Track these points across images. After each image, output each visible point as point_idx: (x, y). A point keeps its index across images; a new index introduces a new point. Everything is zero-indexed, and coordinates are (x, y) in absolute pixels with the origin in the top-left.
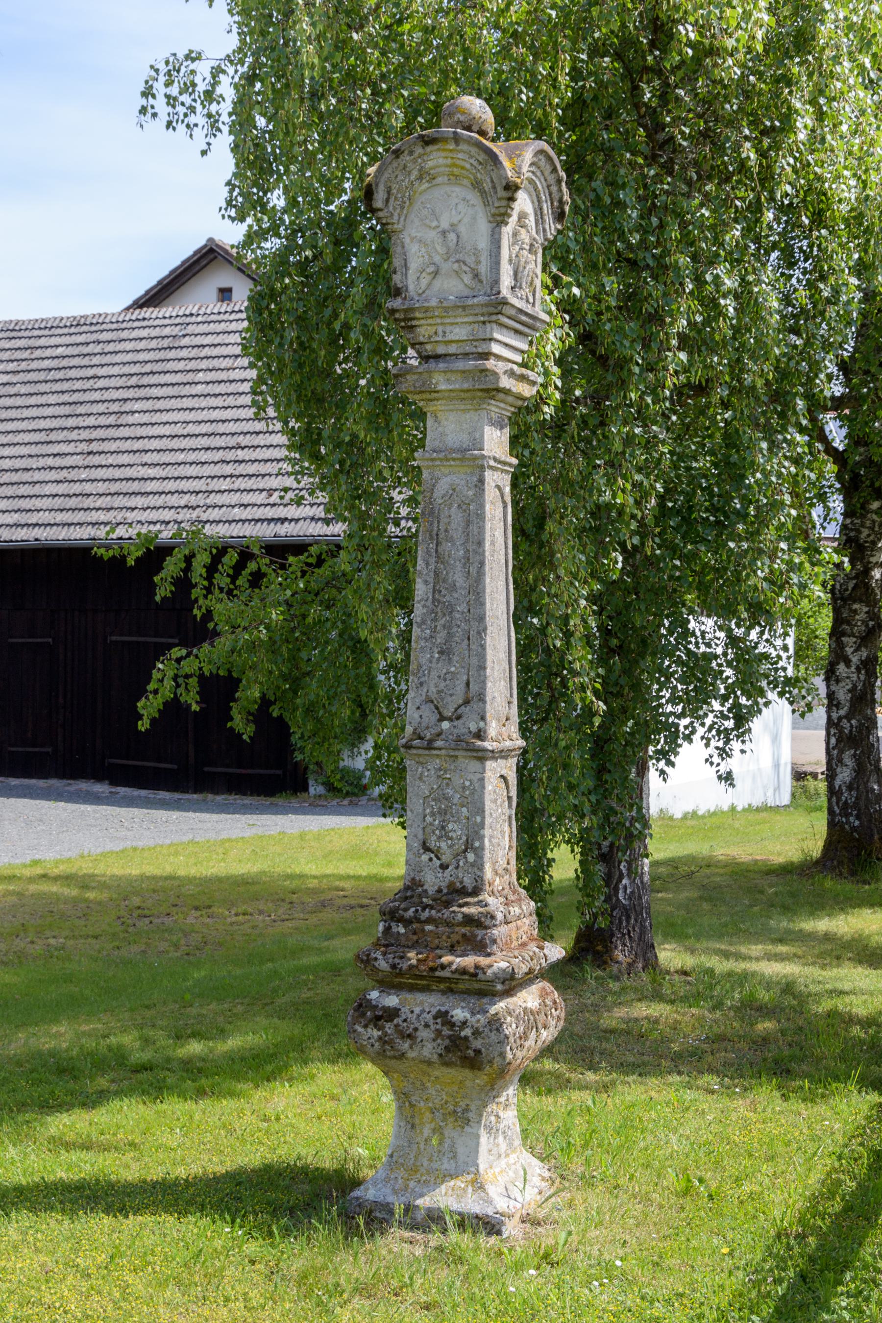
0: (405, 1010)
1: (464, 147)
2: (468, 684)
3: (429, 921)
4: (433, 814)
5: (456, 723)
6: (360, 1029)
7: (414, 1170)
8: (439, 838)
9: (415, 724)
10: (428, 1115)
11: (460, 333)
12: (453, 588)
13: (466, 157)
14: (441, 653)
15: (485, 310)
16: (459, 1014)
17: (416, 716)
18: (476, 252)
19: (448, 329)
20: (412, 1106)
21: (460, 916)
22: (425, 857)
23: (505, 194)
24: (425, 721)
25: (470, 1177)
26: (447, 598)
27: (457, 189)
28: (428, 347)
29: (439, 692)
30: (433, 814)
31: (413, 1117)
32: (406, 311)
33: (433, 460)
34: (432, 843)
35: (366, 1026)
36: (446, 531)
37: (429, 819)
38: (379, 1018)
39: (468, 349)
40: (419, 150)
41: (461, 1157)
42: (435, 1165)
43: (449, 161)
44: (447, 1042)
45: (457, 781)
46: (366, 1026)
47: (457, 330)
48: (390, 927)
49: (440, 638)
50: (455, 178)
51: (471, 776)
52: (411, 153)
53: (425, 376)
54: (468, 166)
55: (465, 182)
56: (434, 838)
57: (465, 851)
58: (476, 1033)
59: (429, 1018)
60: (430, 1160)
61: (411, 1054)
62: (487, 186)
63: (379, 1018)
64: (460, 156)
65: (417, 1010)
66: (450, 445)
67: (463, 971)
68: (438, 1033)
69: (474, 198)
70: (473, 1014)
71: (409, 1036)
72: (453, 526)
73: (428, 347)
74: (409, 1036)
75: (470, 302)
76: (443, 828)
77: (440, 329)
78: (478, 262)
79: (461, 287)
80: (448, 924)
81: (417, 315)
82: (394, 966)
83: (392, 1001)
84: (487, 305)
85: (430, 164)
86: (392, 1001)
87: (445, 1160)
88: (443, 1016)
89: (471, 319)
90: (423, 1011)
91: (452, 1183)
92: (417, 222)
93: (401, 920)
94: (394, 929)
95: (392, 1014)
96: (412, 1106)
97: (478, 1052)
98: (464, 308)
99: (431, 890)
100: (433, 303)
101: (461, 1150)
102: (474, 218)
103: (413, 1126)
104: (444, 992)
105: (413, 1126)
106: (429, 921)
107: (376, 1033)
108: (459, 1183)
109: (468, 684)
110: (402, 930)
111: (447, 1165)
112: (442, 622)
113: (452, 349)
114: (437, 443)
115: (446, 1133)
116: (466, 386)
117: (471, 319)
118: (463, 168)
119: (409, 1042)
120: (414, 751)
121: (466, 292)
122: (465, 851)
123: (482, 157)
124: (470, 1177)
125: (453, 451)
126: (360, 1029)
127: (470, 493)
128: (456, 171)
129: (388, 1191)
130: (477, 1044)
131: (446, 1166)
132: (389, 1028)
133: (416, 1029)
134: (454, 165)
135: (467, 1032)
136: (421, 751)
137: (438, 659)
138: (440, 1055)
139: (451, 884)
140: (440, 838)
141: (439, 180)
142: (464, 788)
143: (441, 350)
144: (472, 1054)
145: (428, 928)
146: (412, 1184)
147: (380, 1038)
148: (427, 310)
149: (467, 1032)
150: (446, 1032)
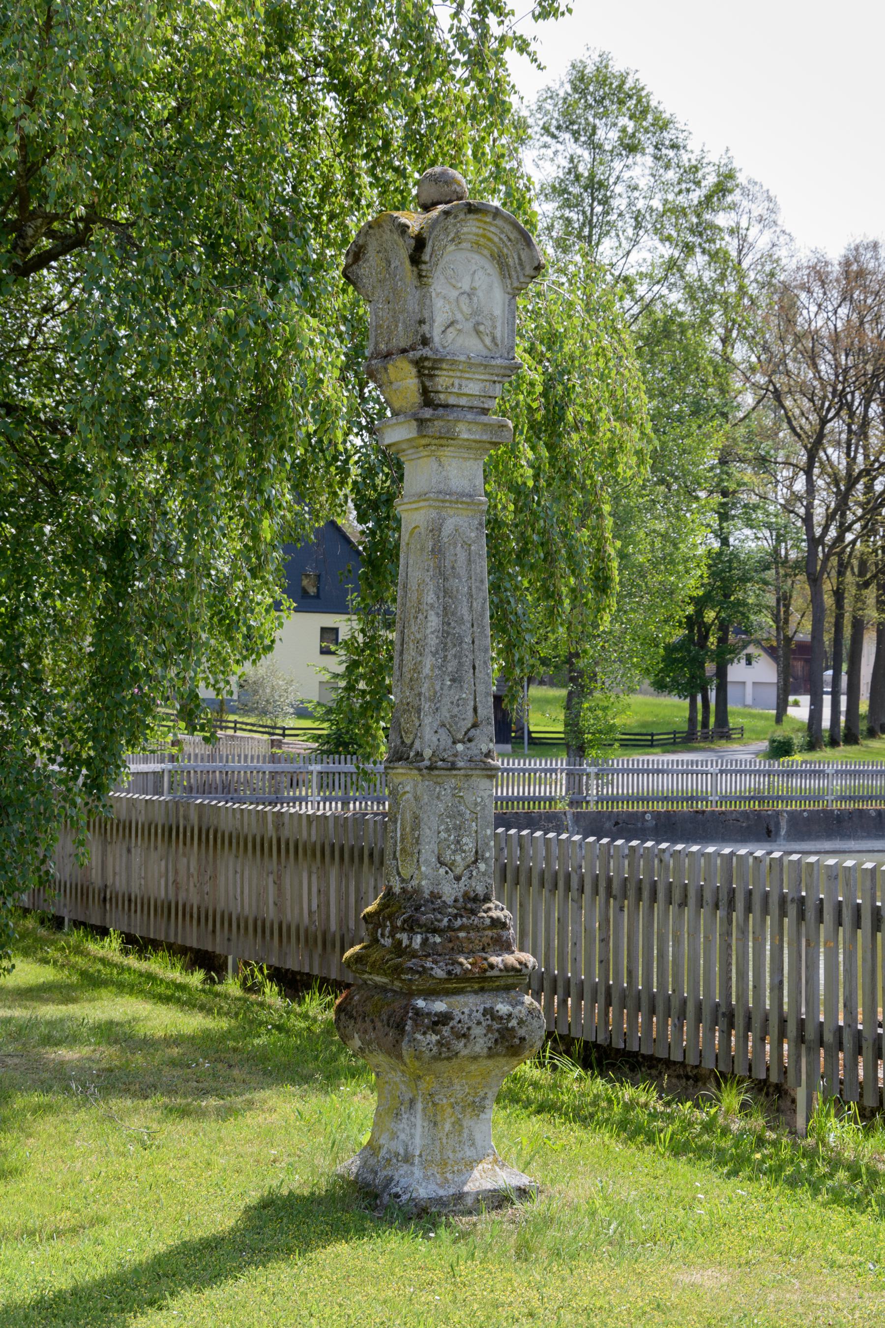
0: (456, 1012)
1: (499, 222)
2: (475, 710)
3: (462, 928)
4: (447, 830)
5: (469, 745)
6: (419, 1036)
7: (444, 1163)
8: (454, 852)
9: (434, 747)
10: (449, 1110)
11: (473, 388)
12: (461, 621)
13: (497, 231)
14: (453, 680)
15: (502, 371)
16: (503, 1008)
17: (435, 739)
18: (493, 318)
19: (464, 383)
20: (435, 1104)
21: (488, 921)
22: (442, 871)
23: (533, 273)
24: (443, 742)
25: (491, 1158)
26: (457, 630)
27: (477, 257)
28: (442, 396)
29: (452, 717)
30: (447, 830)
31: (435, 1115)
32: (435, 361)
33: (443, 501)
34: (448, 856)
35: (424, 1033)
36: (453, 568)
37: (443, 835)
38: (435, 1023)
39: (475, 403)
40: (462, 216)
41: (479, 1143)
42: (459, 1155)
43: (481, 231)
44: (496, 1035)
45: (470, 798)
46: (424, 1033)
47: (471, 385)
48: (427, 939)
49: (451, 666)
50: (477, 247)
51: (482, 793)
52: (456, 217)
53: (451, 424)
54: (496, 240)
55: (486, 252)
56: (449, 852)
57: (475, 862)
58: (521, 1022)
59: (479, 1015)
60: (454, 1151)
61: (465, 1052)
62: (512, 261)
63: (435, 1023)
64: (493, 229)
65: (466, 1010)
66: (454, 489)
67: (508, 968)
68: (489, 1028)
69: (492, 269)
70: (513, 1006)
71: (464, 1035)
72: (459, 564)
73: (442, 396)
74: (464, 1035)
75: (493, 362)
76: (458, 842)
77: (457, 382)
78: (495, 327)
79: (480, 346)
80: (477, 929)
81: (444, 366)
82: (449, 973)
83: (440, 1006)
84: (505, 368)
85: (465, 230)
86: (440, 1006)
87: (466, 1148)
88: (489, 1012)
89: (486, 377)
90: (471, 1011)
91: (480, 1167)
92: (442, 279)
93: (435, 931)
94: (431, 940)
95: (445, 1018)
96: (435, 1104)
97: (523, 1039)
98: (486, 366)
99: (449, 901)
100: (463, 358)
101: (478, 1136)
102: (491, 287)
103: (435, 1124)
104: (476, 992)
105: (435, 1124)
106: (462, 928)
107: (435, 1038)
108: (485, 1165)
109: (475, 710)
110: (438, 940)
111: (469, 1153)
112: (453, 651)
113: (463, 401)
114: (442, 486)
115: (465, 1124)
116: (485, 438)
117: (486, 377)
118: (490, 239)
119: (463, 1041)
120: (437, 772)
121: (485, 352)
122: (475, 862)
123: (514, 235)
124: (491, 1158)
125: (462, 495)
126: (419, 1036)
127: (473, 535)
128: (482, 241)
129: (433, 1187)
130: (522, 1032)
131: (468, 1153)
132: (446, 1031)
133: (469, 1028)
134: (484, 236)
135: (513, 1023)
136: (443, 772)
137: (450, 687)
138: (490, 1048)
139: (466, 895)
140: (454, 852)
141: (464, 245)
142: (476, 804)
143: (452, 400)
144: (517, 1041)
145: (462, 934)
146: (449, 1176)
147: (438, 1042)
148: (454, 362)
149: (513, 1023)
150: (496, 1026)
